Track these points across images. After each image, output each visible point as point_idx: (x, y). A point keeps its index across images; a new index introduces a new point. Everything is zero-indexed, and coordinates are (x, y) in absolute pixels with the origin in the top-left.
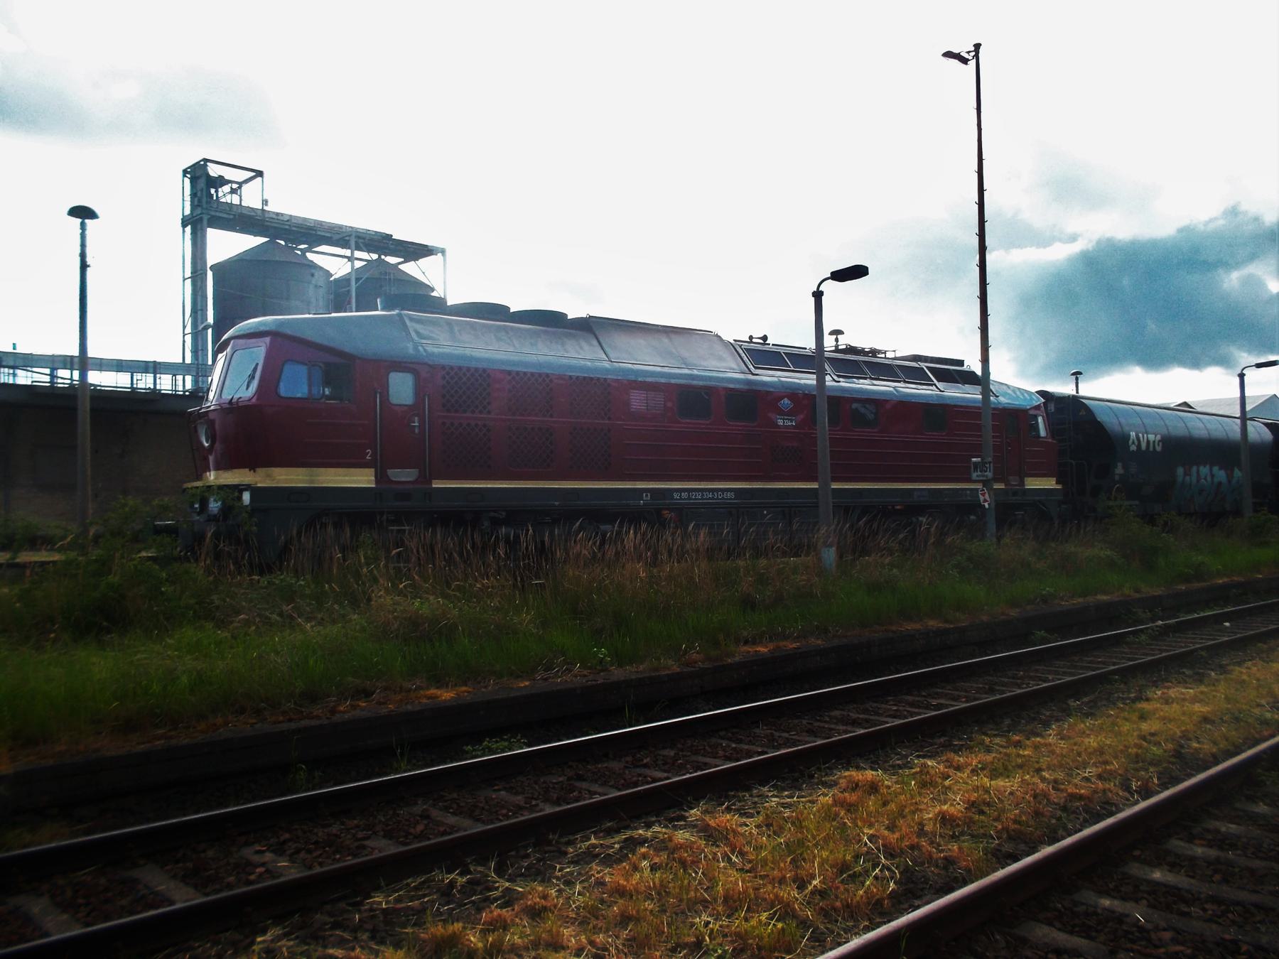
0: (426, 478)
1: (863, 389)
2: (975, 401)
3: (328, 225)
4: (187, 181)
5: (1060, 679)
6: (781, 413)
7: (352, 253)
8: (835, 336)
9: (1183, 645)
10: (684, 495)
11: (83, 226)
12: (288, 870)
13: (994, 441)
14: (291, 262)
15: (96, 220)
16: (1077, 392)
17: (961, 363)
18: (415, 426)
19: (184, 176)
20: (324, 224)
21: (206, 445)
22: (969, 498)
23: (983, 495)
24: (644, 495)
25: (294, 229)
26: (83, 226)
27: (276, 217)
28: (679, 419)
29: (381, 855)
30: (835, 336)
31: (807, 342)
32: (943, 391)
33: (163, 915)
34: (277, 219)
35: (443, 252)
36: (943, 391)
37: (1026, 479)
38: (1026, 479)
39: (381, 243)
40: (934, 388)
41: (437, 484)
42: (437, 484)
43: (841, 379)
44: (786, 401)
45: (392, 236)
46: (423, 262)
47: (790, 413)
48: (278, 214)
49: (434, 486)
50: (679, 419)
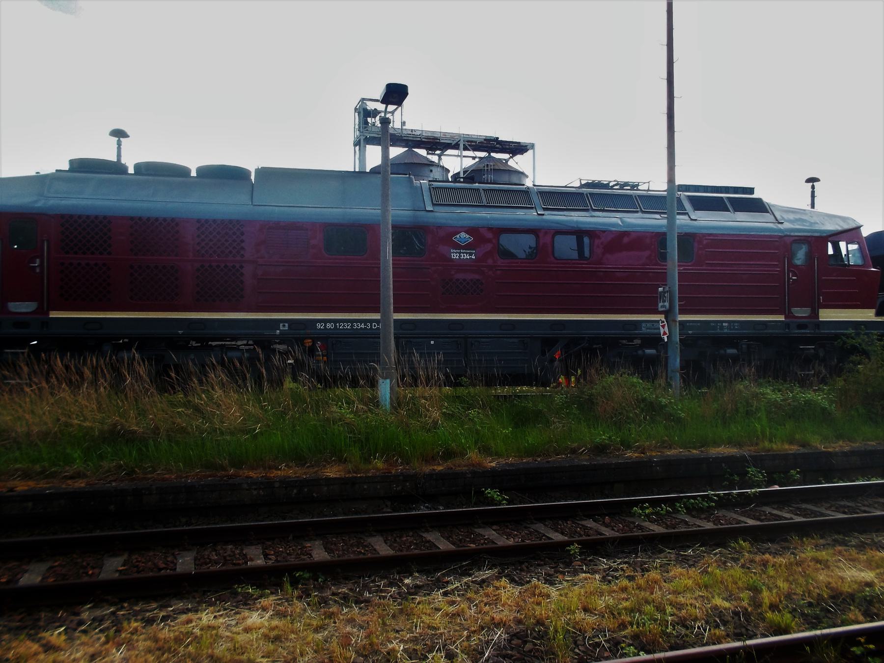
0: (42, 311)
1: (573, 221)
2: (661, 226)
3: (450, 134)
4: (357, 114)
5: (865, 512)
6: (457, 246)
7: (461, 153)
8: (812, 184)
9: (382, 548)
10: (329, 326)
11: (119, 144)
12: (444, 546)
13: (665, 269)
14: (500, 169)
15: (819, 182)
16: (813, 206)
17: (751, 191)
18: (36, 266)
19: (355, 112)
20: (447, 134)
21: (821, 297)
22: (726, 331)
23: (663, 326)
24: (281, 324)
25: (424, 140)
26: (119, 144)
27: (411, 133)
28: (659, 262)
29: (408, 553)
30: (118, 139)
31: (658, 185)
32: (782, 223)
33: (854, 517)
34: (413, 134)
35: (532, 146)
36: (696, 220)
37: (821, 310)
38: (821, 310)
39: (491, 145)
40: (686, 217)
41: (54, 315)
42: (54, 315)
43: (546, 213)
44: (463, 235)
45: (498, 138)
46: (518, 158)
47: (468, 247)
48: (412, 131)
49: (50, 316)
50: (659, 262)
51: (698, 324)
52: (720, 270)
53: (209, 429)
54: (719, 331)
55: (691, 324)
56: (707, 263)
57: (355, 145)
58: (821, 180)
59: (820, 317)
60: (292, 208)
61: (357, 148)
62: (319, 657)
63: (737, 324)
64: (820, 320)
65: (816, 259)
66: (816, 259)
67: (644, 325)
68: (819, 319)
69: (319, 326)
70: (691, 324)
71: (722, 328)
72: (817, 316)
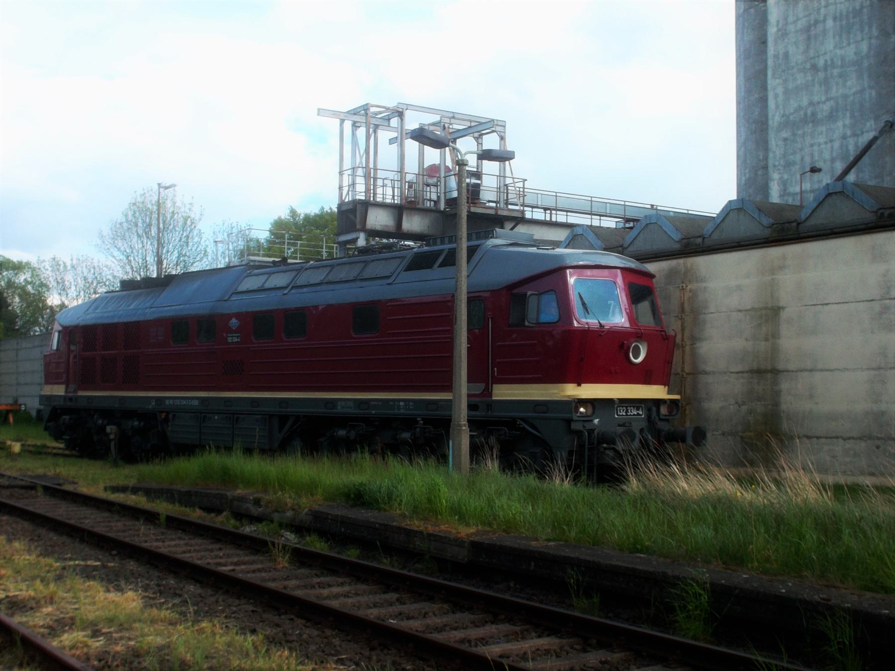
22: (402, 411)
38: (495, 386)
51: (380, 403)
52: (405, 340)
53: (416, 546)
54: (396, 411)
55: (375, 403)
56: (389, 333)
57: (652, 206)
58: (822, 168)
59: (493, 396)
60: (842, 305)
61: (649, 207)
62: (112, 589)
63: (411, 403)
64: (494, 398)
65: (490, 319)
66: (490, 319)
67: (339, 403)
68: (492, 397)
69: (167, 402)
70: (375, 403)
71: (399, 408)
72: (490, 395)
